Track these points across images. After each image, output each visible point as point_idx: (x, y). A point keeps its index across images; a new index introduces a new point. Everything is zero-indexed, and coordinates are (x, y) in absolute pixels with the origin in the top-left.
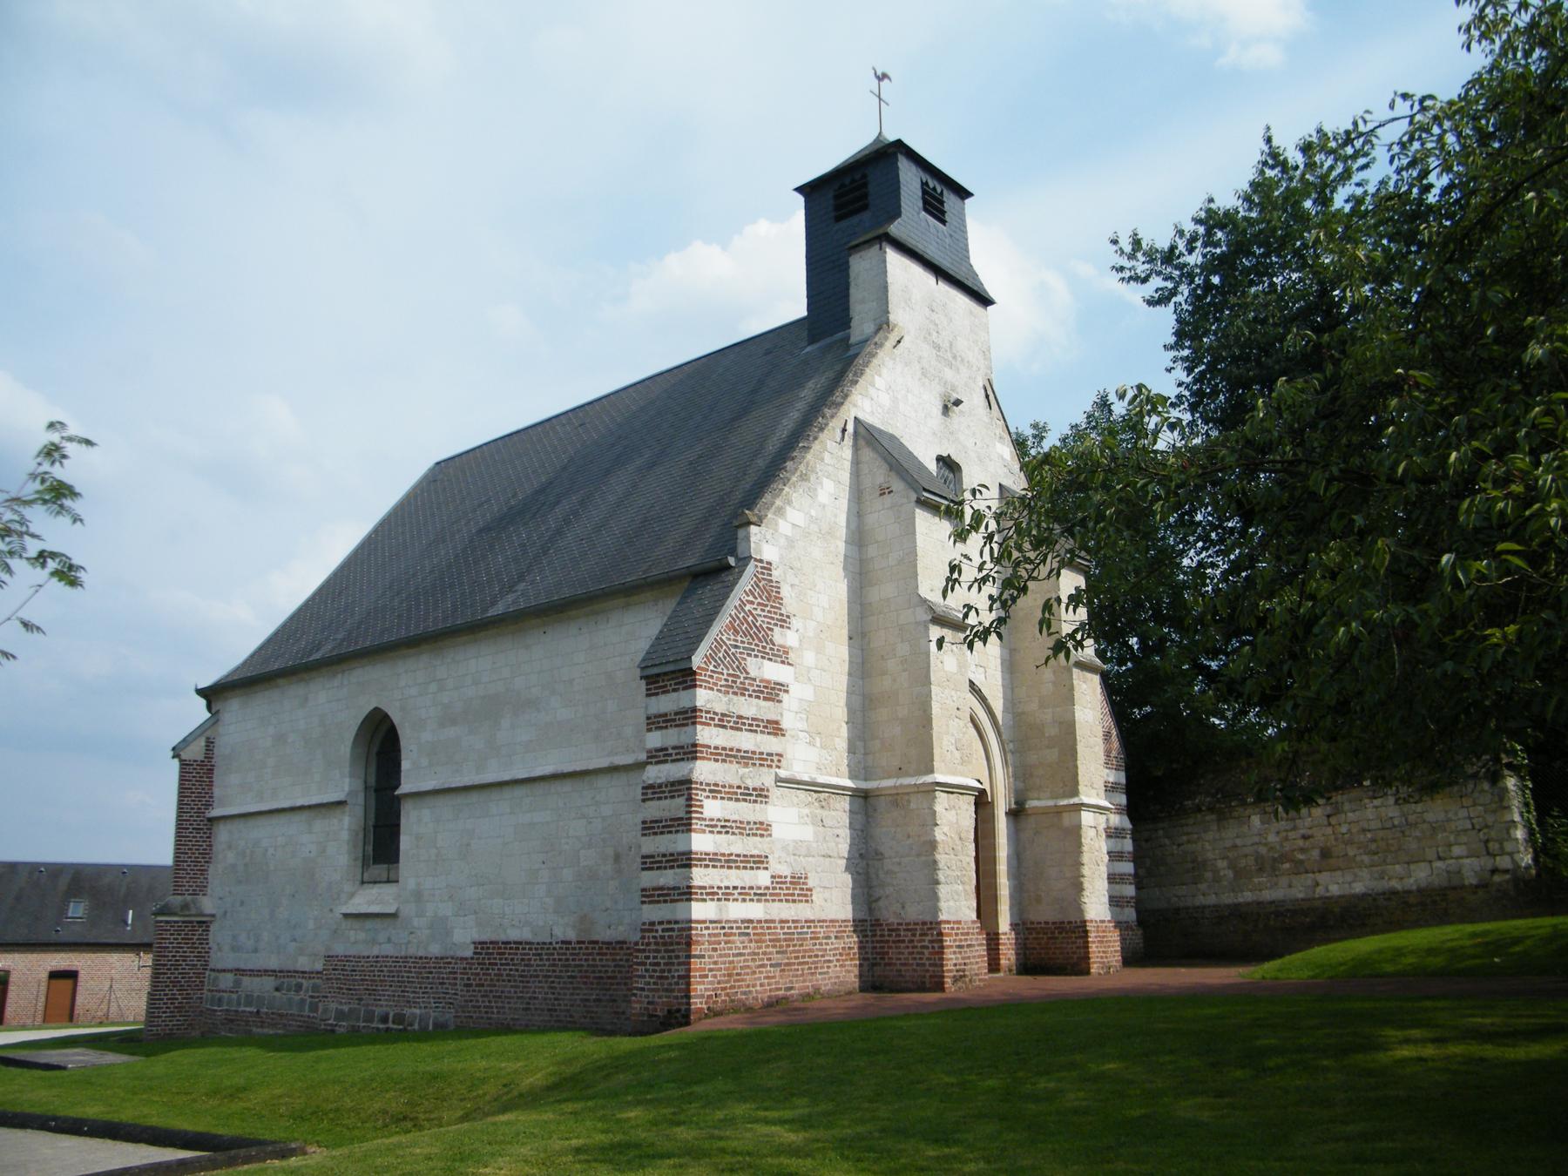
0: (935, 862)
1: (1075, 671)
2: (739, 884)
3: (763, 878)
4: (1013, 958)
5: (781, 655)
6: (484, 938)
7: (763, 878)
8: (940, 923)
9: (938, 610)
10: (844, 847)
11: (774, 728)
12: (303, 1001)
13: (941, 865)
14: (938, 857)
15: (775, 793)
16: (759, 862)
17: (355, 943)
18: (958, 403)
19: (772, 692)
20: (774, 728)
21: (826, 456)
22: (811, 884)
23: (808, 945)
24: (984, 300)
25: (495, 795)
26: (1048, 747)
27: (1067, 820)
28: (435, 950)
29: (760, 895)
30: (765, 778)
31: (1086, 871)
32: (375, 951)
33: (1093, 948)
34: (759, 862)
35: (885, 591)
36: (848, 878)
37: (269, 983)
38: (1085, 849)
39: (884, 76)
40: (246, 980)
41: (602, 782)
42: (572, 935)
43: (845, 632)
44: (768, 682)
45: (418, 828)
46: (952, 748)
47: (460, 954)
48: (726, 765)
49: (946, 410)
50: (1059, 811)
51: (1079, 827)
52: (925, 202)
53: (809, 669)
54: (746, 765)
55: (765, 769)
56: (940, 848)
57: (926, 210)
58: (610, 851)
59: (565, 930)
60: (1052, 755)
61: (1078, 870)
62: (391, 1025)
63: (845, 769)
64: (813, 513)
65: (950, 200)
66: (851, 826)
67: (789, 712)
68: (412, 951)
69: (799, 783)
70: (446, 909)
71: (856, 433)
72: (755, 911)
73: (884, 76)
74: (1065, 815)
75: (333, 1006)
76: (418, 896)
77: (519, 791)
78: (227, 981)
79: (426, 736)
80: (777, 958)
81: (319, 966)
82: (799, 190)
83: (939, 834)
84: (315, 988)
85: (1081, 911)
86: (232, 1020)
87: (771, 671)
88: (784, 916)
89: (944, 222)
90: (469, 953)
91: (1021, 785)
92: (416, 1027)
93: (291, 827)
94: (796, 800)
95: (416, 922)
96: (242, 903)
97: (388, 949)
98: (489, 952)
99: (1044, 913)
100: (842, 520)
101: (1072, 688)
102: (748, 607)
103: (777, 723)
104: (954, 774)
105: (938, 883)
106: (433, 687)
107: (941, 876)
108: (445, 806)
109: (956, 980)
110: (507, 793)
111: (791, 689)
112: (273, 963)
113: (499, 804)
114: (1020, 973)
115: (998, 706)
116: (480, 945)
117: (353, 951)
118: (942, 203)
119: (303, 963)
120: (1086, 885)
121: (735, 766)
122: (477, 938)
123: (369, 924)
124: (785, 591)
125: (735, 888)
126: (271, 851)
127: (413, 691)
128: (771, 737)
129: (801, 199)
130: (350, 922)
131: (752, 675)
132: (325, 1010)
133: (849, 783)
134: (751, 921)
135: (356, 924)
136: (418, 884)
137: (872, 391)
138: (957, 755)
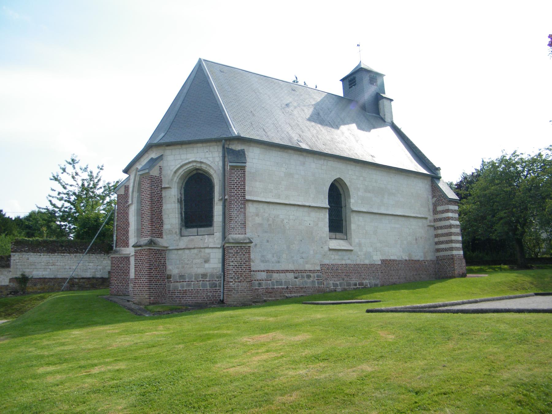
6: (384, 259)
12: (313, 282)
17: (335, 259)
25: (384, 217)
28: (367, 262)
32: (344, 262)
37: (291, 276)
40: (275, 275)
41: (412, 220)
42: (407, 258)
45: (356, 224)
47: (376, 263)
58: (415, 238)
59: (405, 257)
62: (358, 286)
68: (358, 262)
70: (370, 250)
75: (331, 282)
76: (360, 245)
77: (391, 218)
78: (264, 275)
79: (360, 193)
81: (318, 268)
82: (341, 80)
84: (318, 276)
86: (270, 292)
90: (380, 263)
92: (369, 286)
93: (300, 213)
95: (359, 253)
96: (268, 241)
97: (348, 262)
98: (386, 263)
106: (361, 178)
108: (368, 217)
110: (387, 217)
112: (291, 267)
113: (385, 220)
116: (383, 261)
117: (333, 262)
119: (308, 267)
122: (382, 259)
123: (340, 253)
126: (285, 221)
127: (355, 177)
129: (341, 82)
130: (331, 252)
132: (328, 284)
135: (334, 253)
136: (359, 241)
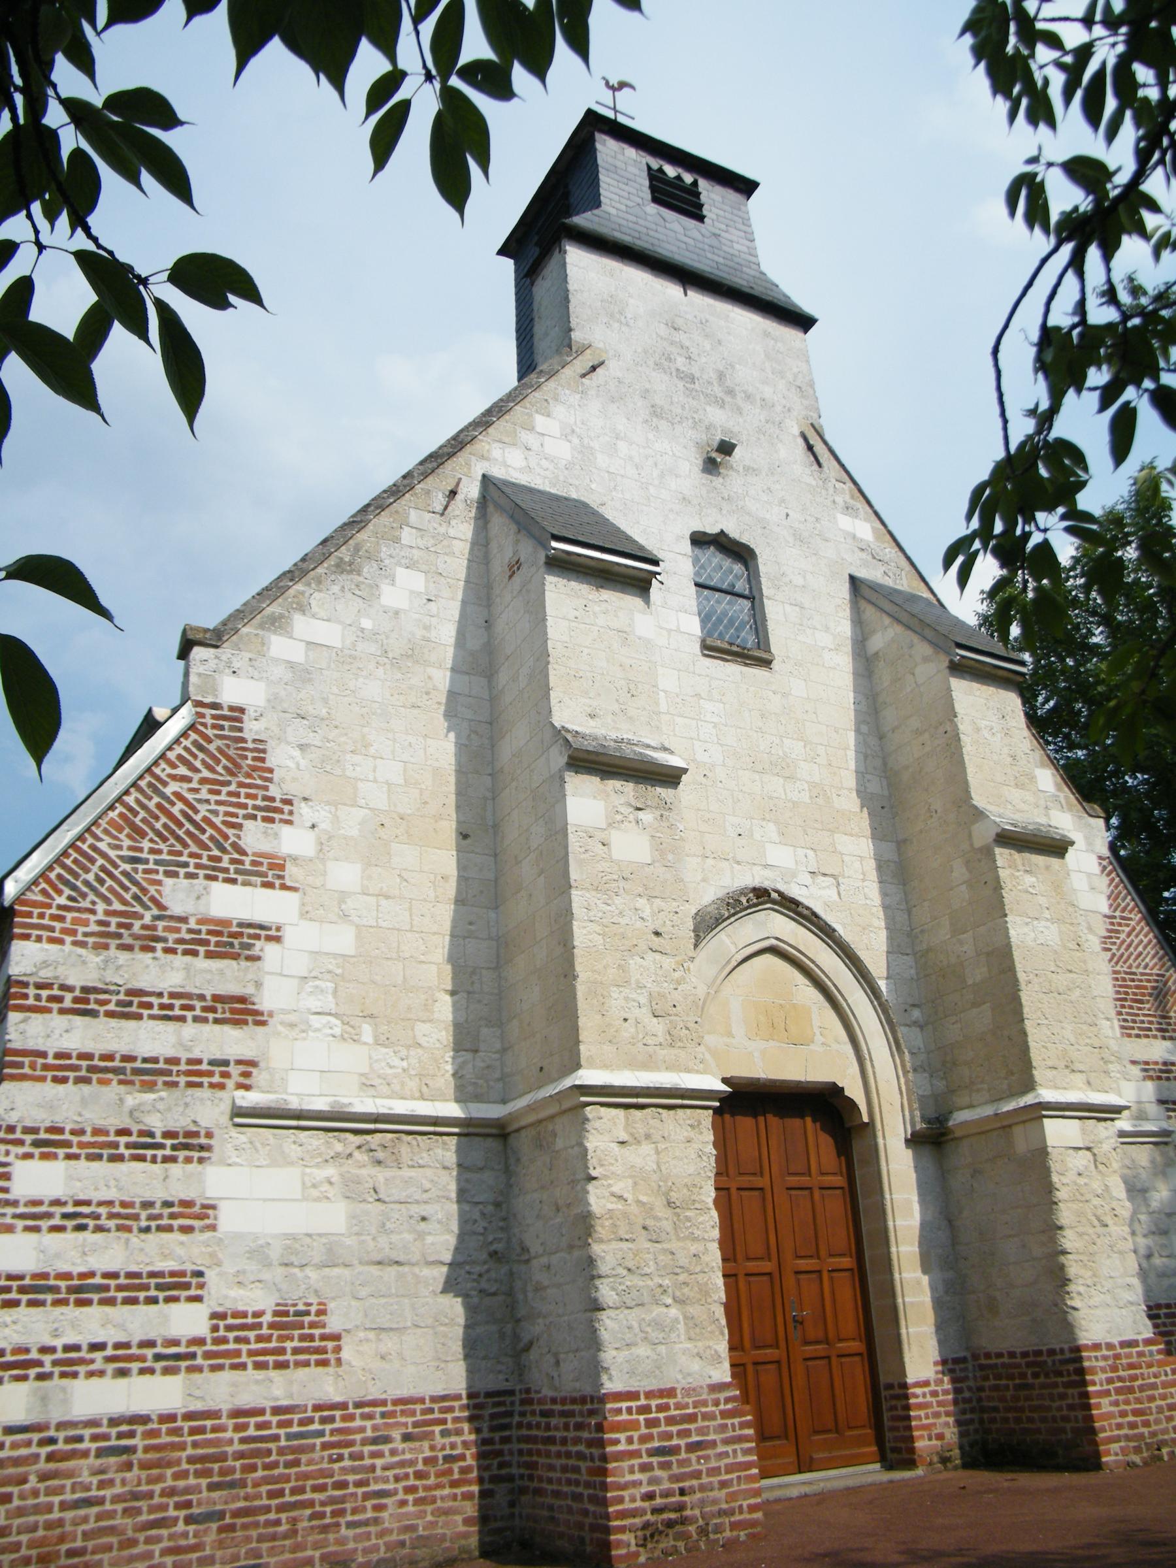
0: (591, 1261)
1: (1002, 855)
2: (111, 1336)
3: (186, 1321)
4: (951, 1434)
5: (271, 873)
7: (186, 1321)
8: (603, 1399)
9: (576, 743)
10: (443, 1240)
11: (240, 1011)
13: (603, 1268)
14: (597, 1249)
15: (232, 1142)
16: (178, 1285)
18: (726, 448)
19: (235, 941)
20: (240, 1011)
21: (407, 536)
22: (334, 1324)
23: (317, 1460)
24: (804, 322)
26: (975, 1005)
27: (1021, 1141)
29: (174, 1358)
30: (207, 1109)
31: (1069, 1240)
33: (1103, 1406)
34: (178, 1285)
35: (517, 738)
36: (455, 1308)
38: (1061, 1194)
39: (622, 85)
43: (449, 827)
44: (226, 923)
46: (644, 1015)
48: (85, 1089)
49: (711, 466)
50: (1004, 1125)
51: (1042, 1152)
52: (653, 188)
53: (343, 896)
54: (150, 1087)
55: (205, 1093)
56: (602, 1229)
57: (655, 200)
60: (981, 1018)
61: (1053, 1240)
63: (444, 1078)
64: (367, 624)
65: (711, 194)
66: (463, 1195)
67: (276, 979)
69: (299, 1115)
71: (484, 503)
72: (159, 1394)
73: (622, 85)
74: (1018, 1131)
80: (207, 1499)
82: (501, 252)
83: (598, 1200)
85: (1068, 1328)
87: (230, 902)
88: (246, 1400)
89: (701, 218)
91: (941, 1085)
94: (294, 1151)
99: (1006, 1335)
100: (447, 633)
101: (998, 887)
102: (172, 788)
103: (242, 1000)
104: (648, 1064)
105: (597, 1307)
107: (606, 1292)
109: (650, 1534)
111: (288, 934)
114: (970, 1463)
115: (874, 948)
118: (698, 195)
120: (1072, 1270)
121: (114, 1090)
124: (281, 758)
125: (96, 1347)
128: (227, 1029)
131: (176, 909)
133: (454, 1110)
134: (144, 1419)
137: (525, 437)
138: (658, 1027)
